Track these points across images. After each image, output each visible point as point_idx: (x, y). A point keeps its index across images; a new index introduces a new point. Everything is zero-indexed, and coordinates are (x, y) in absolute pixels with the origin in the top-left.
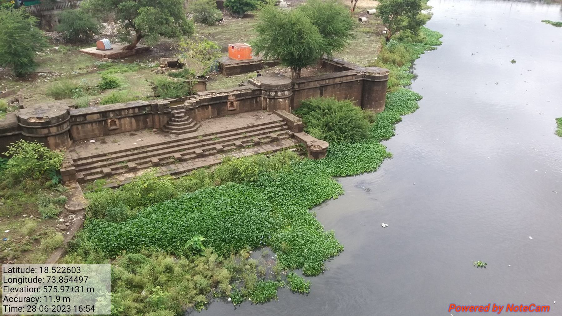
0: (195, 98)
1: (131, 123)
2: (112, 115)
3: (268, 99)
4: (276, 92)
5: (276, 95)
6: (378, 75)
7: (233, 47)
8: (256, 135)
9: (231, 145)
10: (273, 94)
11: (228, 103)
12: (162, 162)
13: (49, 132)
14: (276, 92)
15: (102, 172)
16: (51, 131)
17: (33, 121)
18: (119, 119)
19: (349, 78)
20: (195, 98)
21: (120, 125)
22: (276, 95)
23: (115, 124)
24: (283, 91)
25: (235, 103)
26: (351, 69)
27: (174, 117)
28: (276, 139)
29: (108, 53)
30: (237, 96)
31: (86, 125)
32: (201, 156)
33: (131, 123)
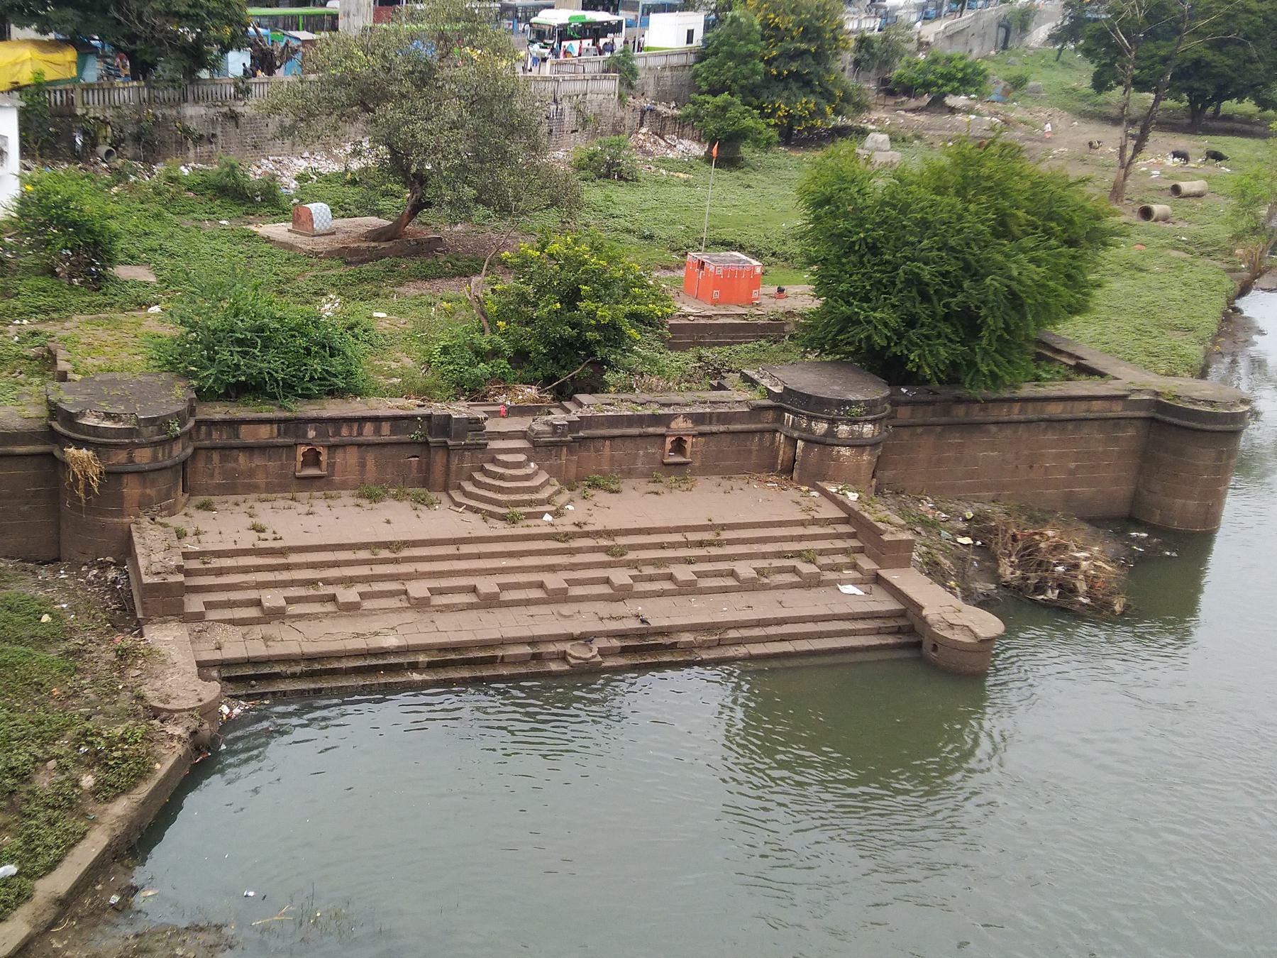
0: (568, 411)
1: (363, 465)
2: (312, 434)
3: (800, 444)
4: (833, 422)
5: (830, 433)
6: (1208, 409)
7: (702, 265)
8: (689, 561)
9: (530, 585)
10: (821, 428)
11: (669, 440)
12: (439, 600)
13: (131, 460)
14: (833, 422)
15: (258, 603)
16: (137, 460)
17: (91, 421)
18: (332, 448)
19: (1096, 405)
20: (568, 411)
21: (331, 466)
22: (830, 433)
23: (317, 463)
24: (856, 422)
25: (689, 440)
26: (1102, 375)
27: (494, 461)
28: (276, 615)
29: (322, 244)
30: (698, 419)
31: (235, 452)
32: (559, 597)
33: (363, 465)
